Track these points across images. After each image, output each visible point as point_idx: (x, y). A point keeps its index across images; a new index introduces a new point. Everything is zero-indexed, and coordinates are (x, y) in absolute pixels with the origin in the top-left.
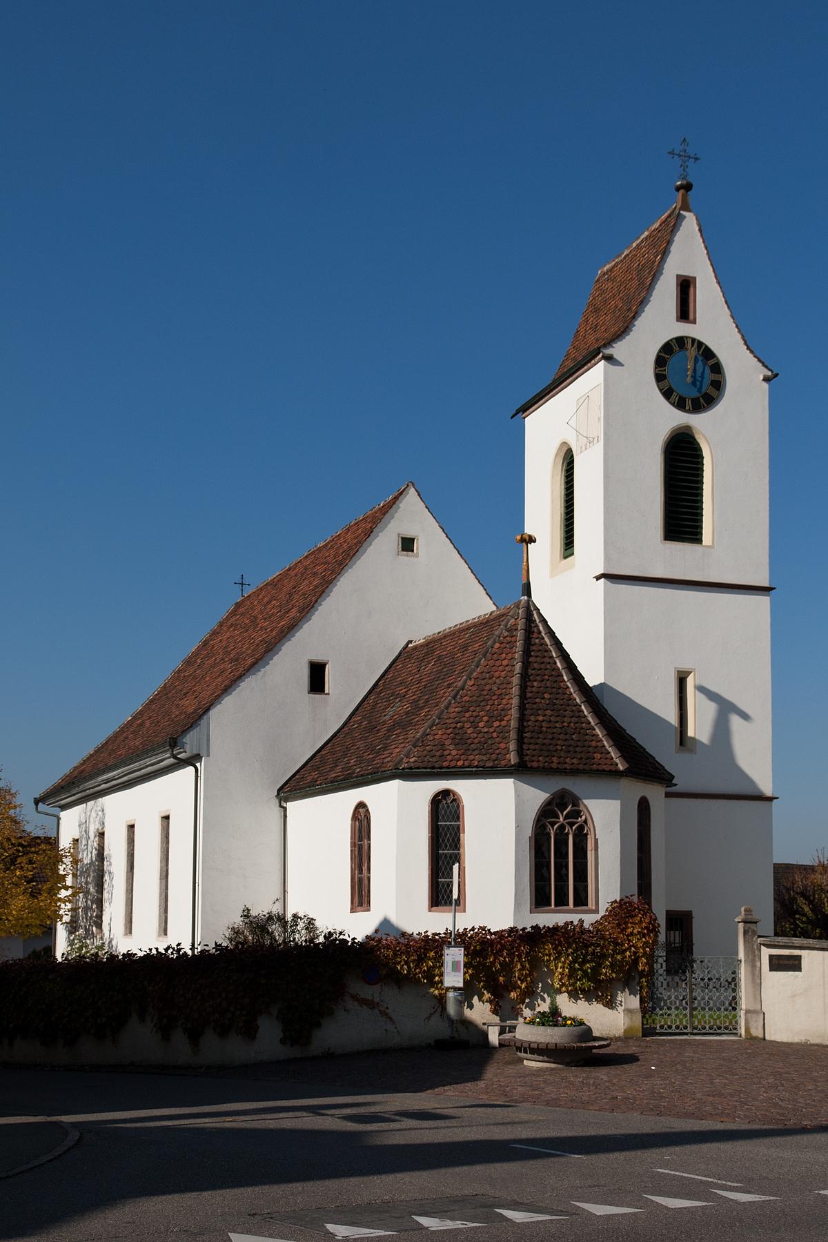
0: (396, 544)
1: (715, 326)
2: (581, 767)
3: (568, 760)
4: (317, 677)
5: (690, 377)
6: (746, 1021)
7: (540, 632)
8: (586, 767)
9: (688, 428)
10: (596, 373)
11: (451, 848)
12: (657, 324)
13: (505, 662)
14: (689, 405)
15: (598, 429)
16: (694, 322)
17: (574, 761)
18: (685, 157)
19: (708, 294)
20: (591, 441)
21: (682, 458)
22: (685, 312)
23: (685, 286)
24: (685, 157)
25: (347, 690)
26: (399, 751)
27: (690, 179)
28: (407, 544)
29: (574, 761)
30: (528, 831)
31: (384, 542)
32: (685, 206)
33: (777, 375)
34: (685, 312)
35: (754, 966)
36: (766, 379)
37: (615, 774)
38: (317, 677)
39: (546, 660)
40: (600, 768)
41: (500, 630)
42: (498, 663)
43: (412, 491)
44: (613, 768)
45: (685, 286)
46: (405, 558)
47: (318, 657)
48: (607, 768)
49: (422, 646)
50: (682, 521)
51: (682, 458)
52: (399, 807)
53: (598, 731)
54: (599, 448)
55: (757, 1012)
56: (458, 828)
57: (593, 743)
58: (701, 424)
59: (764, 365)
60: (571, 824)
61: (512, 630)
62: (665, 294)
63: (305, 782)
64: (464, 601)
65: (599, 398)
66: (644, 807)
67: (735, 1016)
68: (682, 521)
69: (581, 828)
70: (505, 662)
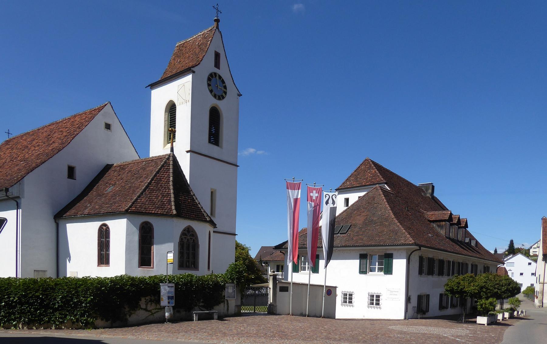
70: (166, 176)
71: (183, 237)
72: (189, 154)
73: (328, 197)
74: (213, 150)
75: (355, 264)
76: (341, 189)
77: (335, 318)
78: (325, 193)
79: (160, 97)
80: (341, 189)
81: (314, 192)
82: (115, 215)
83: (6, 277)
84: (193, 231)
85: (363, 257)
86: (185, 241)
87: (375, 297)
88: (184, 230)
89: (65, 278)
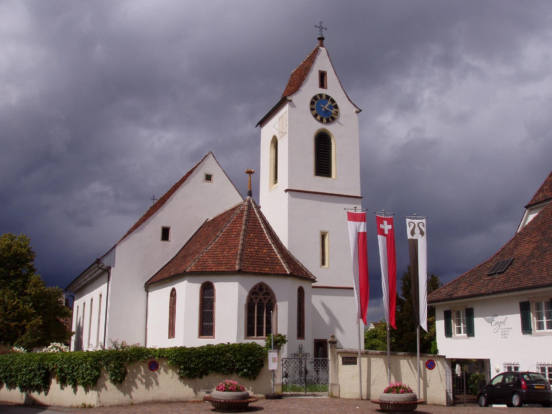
0: (203, 177)
1: (334, 90)
2: (270, 272)
3: (264, 269)
4: (165, 234)
5: (324, 110)
6: (331, 389)
7: (254, 212)
8: (273, 272)
9: (325, 129)
10: (286, 108)
11: (209, 309)
12: (310, 88)
13: (238, 225)
14: (325, 120)
15: (286, 129)
16: (326, 88)
17: (267, 269)
18: (321, 28)
19: (331, 78)
20: (283, 134)
21: (323, 143)
22: (322, 84)
23: (323, 75)
24: (321, 28)
25: (178, 240)
26: (191, 266)
27: (324, 36)
28: (208, 178)
29: (267, 269)
30: (244, 301)
31: (198, 177)
32: (322, 45)
33: (361, 110)
34: (322, 84)
35: (335, 360)
36: (357, 112)
37: (285, 275)
38: (165, 234)
39: (257, 224)
40: (279, 273)
41: (238, 211)
42: (235, 225)
43: (211, 155)
44: (285, 273)
45: (323, 75)
46: (207, 184)
47: (166, 225)
48: (281, 273)
49: (212, 220)
50: (323, 167)
51: (323, 143)
52: (188, 291)
53: (279, 256)
54: (286, 136)
55: (336, 385)
56: (213, 300)
57: (276, 262)
58: (331, 128)
59: (355, 106)
60: (265, 298)
61: (242, 212)
62: (313, 77)
63: (153, 283)
64: (228, 198)
65: (287, 116)
66: (301, 291)
67: (326, 387)
68: (323, 167)
69: (270, 300)
70: (238, 225)
71: (252, 297)
72: (287, 193)
73: (412, 225)
74: (321, 184)
75: (515, 319)
76: (533, 205)
77: (426, 404)
78: (408, 221)
79: (268, 132)
80: (533, 205)
81: (385, 222)
82: (228, 273)
83: (187, 347)
84: (268, 288)
85: (525, 310)
86: (256, 301)
87: (547, 371)
88: (255, 288)
89: (147, 349)
